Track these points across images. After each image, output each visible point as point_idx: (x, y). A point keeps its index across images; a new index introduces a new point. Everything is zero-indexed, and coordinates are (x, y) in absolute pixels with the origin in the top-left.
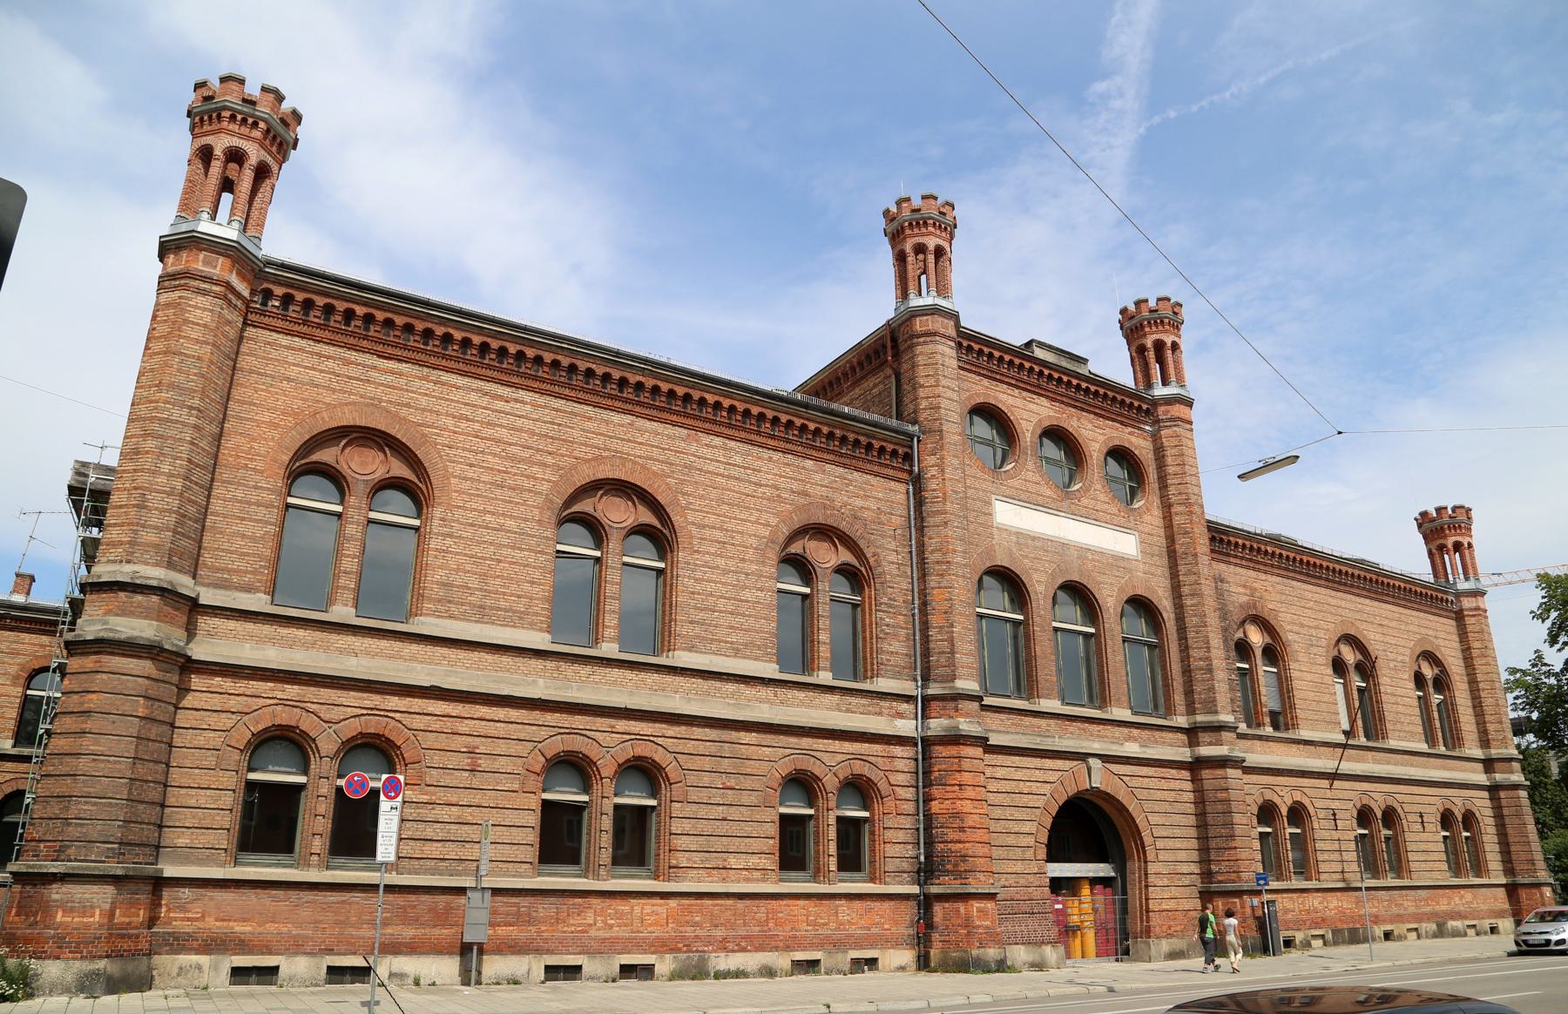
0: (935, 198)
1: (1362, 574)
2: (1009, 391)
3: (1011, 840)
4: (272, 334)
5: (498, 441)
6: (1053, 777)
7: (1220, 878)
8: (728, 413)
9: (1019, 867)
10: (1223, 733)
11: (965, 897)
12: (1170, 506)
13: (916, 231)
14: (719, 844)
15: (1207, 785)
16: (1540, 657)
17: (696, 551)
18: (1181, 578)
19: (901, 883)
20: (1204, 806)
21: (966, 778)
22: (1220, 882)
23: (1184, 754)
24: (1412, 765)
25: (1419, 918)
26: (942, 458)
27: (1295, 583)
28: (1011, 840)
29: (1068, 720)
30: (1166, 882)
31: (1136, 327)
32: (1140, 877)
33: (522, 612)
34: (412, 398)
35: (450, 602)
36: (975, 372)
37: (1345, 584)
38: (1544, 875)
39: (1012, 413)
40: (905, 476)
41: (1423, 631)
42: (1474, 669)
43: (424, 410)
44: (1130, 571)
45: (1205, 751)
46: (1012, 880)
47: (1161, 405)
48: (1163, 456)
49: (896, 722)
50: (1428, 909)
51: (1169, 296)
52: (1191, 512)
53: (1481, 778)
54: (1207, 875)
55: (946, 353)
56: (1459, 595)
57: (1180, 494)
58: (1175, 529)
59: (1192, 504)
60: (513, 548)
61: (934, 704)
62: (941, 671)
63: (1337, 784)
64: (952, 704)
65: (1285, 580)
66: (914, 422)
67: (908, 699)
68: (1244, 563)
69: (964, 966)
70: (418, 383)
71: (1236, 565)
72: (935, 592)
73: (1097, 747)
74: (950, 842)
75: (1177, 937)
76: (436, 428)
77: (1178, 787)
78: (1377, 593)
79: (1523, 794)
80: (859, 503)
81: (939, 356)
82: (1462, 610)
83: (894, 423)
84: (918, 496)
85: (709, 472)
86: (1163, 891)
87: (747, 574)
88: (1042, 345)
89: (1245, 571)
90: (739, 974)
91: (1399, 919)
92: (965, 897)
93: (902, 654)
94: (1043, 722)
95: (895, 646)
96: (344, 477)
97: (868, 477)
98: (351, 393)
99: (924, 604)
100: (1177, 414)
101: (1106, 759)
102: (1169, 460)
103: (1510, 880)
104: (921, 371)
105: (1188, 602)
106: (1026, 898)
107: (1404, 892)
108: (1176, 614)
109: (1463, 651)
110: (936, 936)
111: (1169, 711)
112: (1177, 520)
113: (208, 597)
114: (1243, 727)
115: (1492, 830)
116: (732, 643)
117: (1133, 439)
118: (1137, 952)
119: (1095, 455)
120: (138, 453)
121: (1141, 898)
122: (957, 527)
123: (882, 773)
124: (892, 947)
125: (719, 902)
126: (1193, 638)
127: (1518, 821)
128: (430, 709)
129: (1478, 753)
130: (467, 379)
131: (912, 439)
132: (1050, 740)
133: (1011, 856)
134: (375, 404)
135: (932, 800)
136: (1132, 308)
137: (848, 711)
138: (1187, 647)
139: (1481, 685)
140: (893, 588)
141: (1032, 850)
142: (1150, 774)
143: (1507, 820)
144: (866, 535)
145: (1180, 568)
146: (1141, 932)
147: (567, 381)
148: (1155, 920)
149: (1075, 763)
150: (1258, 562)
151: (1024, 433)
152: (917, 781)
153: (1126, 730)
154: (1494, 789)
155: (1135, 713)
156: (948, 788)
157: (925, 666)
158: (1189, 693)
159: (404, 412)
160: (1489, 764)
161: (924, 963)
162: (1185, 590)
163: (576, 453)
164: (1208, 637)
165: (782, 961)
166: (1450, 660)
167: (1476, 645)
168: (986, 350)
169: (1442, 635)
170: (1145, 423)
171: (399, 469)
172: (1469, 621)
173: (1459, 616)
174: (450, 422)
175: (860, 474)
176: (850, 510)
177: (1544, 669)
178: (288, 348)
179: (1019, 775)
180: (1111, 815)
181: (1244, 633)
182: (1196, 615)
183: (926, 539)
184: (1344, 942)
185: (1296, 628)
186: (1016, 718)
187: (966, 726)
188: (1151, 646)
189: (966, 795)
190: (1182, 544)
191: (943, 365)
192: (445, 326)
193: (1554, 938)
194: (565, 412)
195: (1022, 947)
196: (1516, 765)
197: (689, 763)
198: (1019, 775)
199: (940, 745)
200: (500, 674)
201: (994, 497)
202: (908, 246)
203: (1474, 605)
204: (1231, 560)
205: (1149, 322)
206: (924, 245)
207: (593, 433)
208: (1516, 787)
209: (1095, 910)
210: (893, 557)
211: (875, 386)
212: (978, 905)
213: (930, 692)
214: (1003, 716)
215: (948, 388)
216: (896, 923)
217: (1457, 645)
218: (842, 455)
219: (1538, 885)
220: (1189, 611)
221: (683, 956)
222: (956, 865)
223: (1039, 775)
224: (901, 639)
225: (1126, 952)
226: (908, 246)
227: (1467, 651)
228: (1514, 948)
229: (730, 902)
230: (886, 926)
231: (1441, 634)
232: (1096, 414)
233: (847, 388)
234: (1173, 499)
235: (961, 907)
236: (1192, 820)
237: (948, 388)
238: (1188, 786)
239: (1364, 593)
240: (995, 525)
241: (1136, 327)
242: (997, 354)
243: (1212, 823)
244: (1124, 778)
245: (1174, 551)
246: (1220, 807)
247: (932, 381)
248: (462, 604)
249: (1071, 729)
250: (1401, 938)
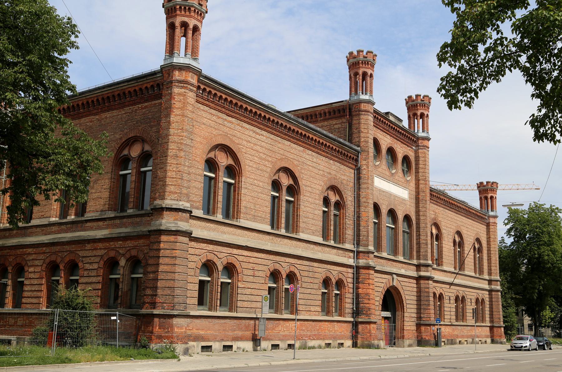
1: (465, 207)
2: (380, 133)
4: (199, 104)
5: (257, 151)
6: (384, 281)
11: (369, 323)
12: (419, 180)
14: (309, 302)
15: (422, 286)
16: (503, 240)
17: (305, 196)
18: (420, 209)
20: (420, 293)
21: (371, 281)
22: (424, 321)
23: (414, 274)
24: (470, 281)
25: (468, 337)
26: (368, 162)
27: (447, 211)
31: (414, 105)
32: (401, 318)
33: (264, 218)
34: (235, 133)
35: (247, 214)
37: (459, 211)
38: (502, 324)
40: (354, 167)
41: (478, 230)
42: (490, 246)
43: (239, 138)
45: (423, 274)
47: (420, 139)
48: (419, 160)
50: (470, 334)
51: (373, 51)
53: (487, 287)
54: (419, 318)
55: (371, 118)
56: (489, 217)
58: (420, 190)
59: (426, 180)
60: (262, 193)
61: (361, 254)
62: (364, 242)
63: (452, 287)
64: (367, 255)
65: (444, 210)
66: (359, 146)
68: (223, 110)
69: (369, 346)
70: (237, 127)
72: (363, 213)
73: (394, 270)
76: (242, 145)
78: (467, 215)
79: (500, 293)
82: (489, 223)
83: (347, 143)
84: (358, 175)
85: (308, 165)
87: (316, 204)
88: (392, 115)
90: (313, 348)
91: (463, 337)
92: (369, 323)
95: (349, 233)
96: (217, 164)
98: (220, 131)
99: (359, 217)
101: (398, 275)
102: (421, 162)
103: (491, 325)
104: (362, 126)
105: (422, 218)
107: (464, 327)
108: (416, 221)
109: (487, 238)
110: (359, 336)
111: (411, 258)
112: (421, 186)
114: (435, 266)
115: (488, 306)
116: (312, 230)
118: (399, 344)
120: (177, 157)
121: (401, 325)
125: (308, 323)
127: (497, 304)
128: (244, 254)
129: (486, 277)
130: (250, 126)
134: (226, 135)
135: (359, 288)
136: (355, 53)
137: (338, 255)
138: (419, 235)
139: (492, 252)
142: (407, 281)
143: (493, 303)
145: (420, 205)
146: (401, 337)
148: (406, 333)
150: (438, 202)
152: (354, 281)
153: (402, 265)
154: (490, 291)
156: (365, 285)
157: (358, 242)
158: (418, 252)
159: (234, 139)
160: (490, 282)
161: (355, 345)
162: (421, 213)
163: (277, 157)
165: (323, 343)
166: (483, 241)
167: (492, 236)
169: (482, 232)
172: (491, 227)
173: (488, 225)
174: (245, 143)
177: (504, 244)
178: (204, 111)
180: (394, 295)
183: (361, 193)
184: (449, 344)
185: (445, 228)
187: (371, 263)
188: (408, 233)
190: (422, 196)
192: (246, 104)
193: (524, 345)
194: (274, 140)
196: (499, 283)
199: (363, 269)
200: (259, 241)
201: (375, 175)
203: (494, 221)
205: (420, 105)
206: (366, 72)
207: (280, 148)
208: (498, 291)
209: (385, 328)
211: (336, 124)
213: (360, 250)
217: (485, 236)
219: (500, 327)
220: (422, 221)
221: (301, 341)
222: (367, 312)
223: (381, 280)
225: (394, 344)
227: (489, 238)
228: (510, 348)
229: (311, 323)
231: (479, 229)
232: (401, 142)
233: (321, 120)
234: (420, 178)
235: (368, 326)
236: (415, 298)
238: (415, 286)
239: (464, 215)
241: (414, 105)
244: (401, 282)
245: (419, 198)
246: (426, 294)
247: (366, 131)
248: (250, 215)
250: (463, 343)
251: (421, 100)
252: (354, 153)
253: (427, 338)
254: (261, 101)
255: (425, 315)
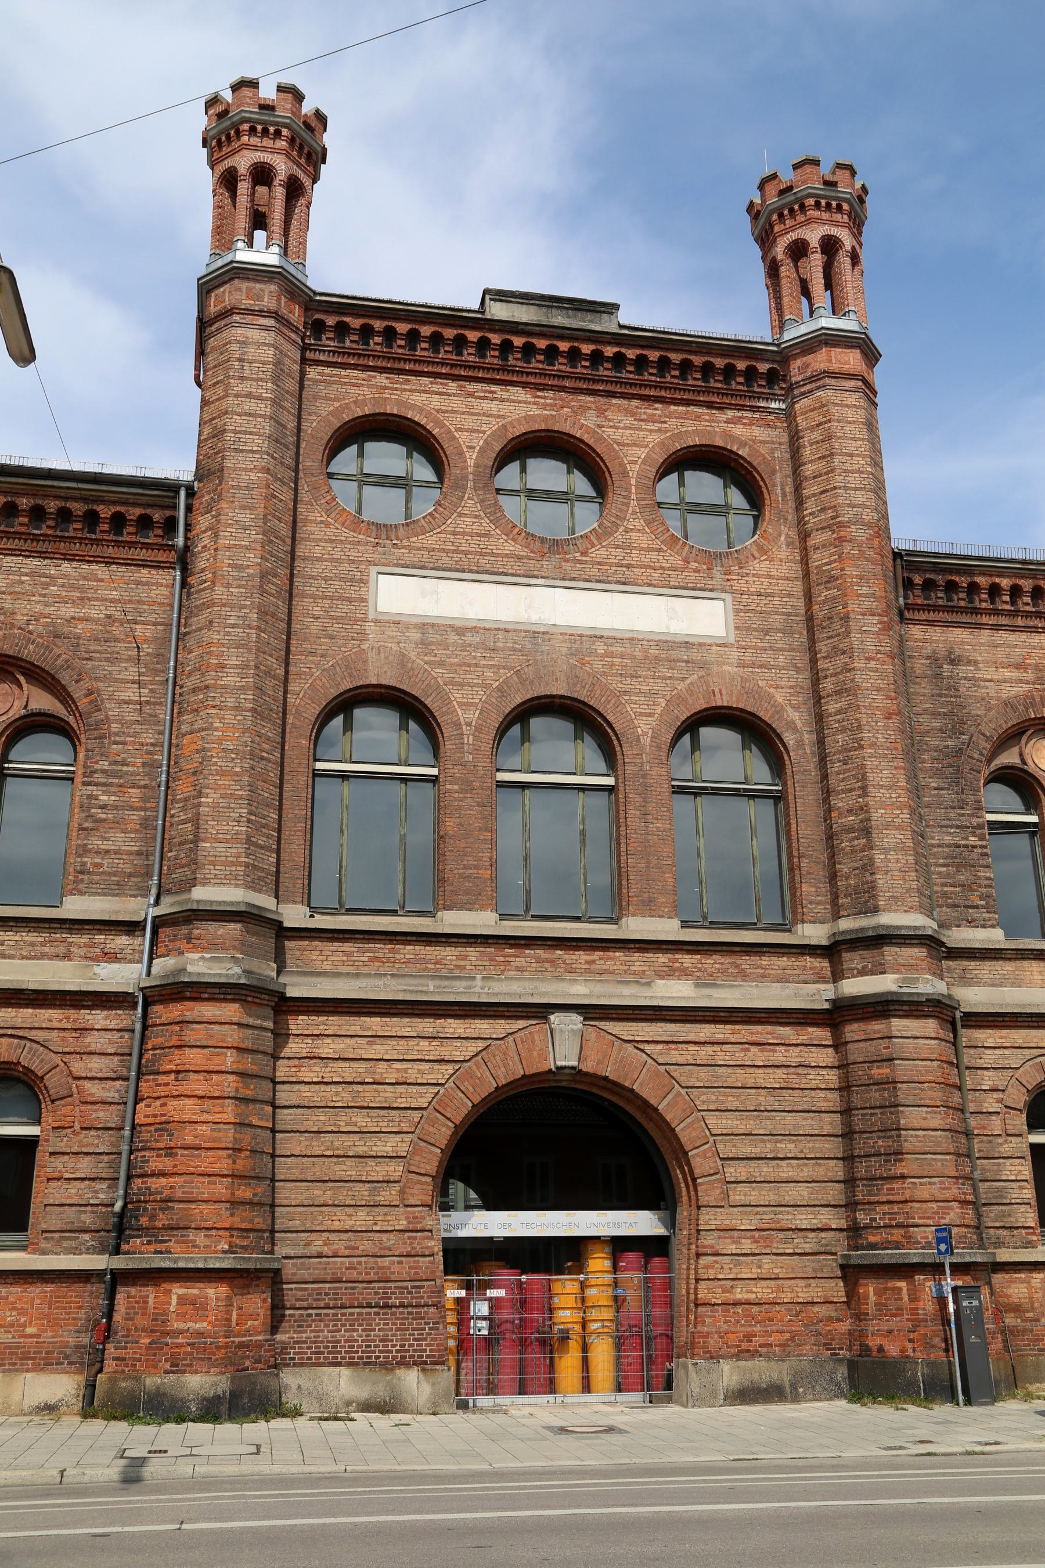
0: (816, 163)
2: (435, 388)
3: (346, 1169)
7: (872, 1239)
8: (923, 590)
9: (361, 1219)
10: (887, 950)
13: (789, 223)
19: (75, 1251)
22: (873, 1246)
28: (346, 1169)
29: (512, 946)
30: (747, 1246)
36: (355, 367)
39: (442, 426)
44: (704, 665)
45: (854, 986)
46: (340, 1244)
47: (795, 357)
49: (97, 970)
52: (841, 539)
57: (823, 510)
64: (184, 930)
67: (132, 927)
68: (1020, 622)
71: (996, 627)
74: (152, 1175)
75: (768, 1357)
77: (794, 1060)
80: (67, 611)
81: (235, 347)
86: (737, 1264)
89: (1024, 636)
93: (129, 853)
94: (449, 954)
97: (93, 567)
100: (822, 366)
101: (591, 1012)
102: (807, 453)
105: (832, 706)
106: (372, 1276)
113: (294, 915)
117: (738, 430)
119: (634, 470)
122: (233, 626)
123: (57, 1059)
124: (37, 1369)
126: (838, 773)
131: (178, 492)
132: (460, 985)
133: (341, 1198)
140: (124, 743)
141: (397, 1187)
142: (719, 1037)
144: (77, 663)
147: (945, 603)
149: (521, 1023)
151: (461, 453)
153: (662, 958)
155: (685, 924)
164: (863, 767)
168: (378, 325)
170: (773, 397)
171: (42, 701)
175: (75, 564)
176: (47, 625)
179: (379, 1049)
181: (1021, 755)
182: (844, 730)
186: (383, 950)
189: (186, 1088)
191: (240, 360)
195: (345, 1372)
197: (78, 1067)
198: (379, 1049)
201: (374, 570)
202: (779, 250)
204: (985, 619)
209: (618, 1302)
210: (130, 693)
212: (182, 1291)
214: (348, 947)
215: (249, 395)
216: (54, 1323)
218: (36, 538)
222: (153, 1217)
224: (129, 827)
226: (779, 250)
230: (29, 1330)
235: (151, 1294)
237: (249, 395)
238: (828, 1056)
240: (371, 615)
242: (402, 328)
243: (860, 1127)
246: (876, 1096)
249: (519, 961)
251: (826, 183)
252: (144, 500)
253: (893, 1350)
254: (16, 462)
255: (879, 1215)
